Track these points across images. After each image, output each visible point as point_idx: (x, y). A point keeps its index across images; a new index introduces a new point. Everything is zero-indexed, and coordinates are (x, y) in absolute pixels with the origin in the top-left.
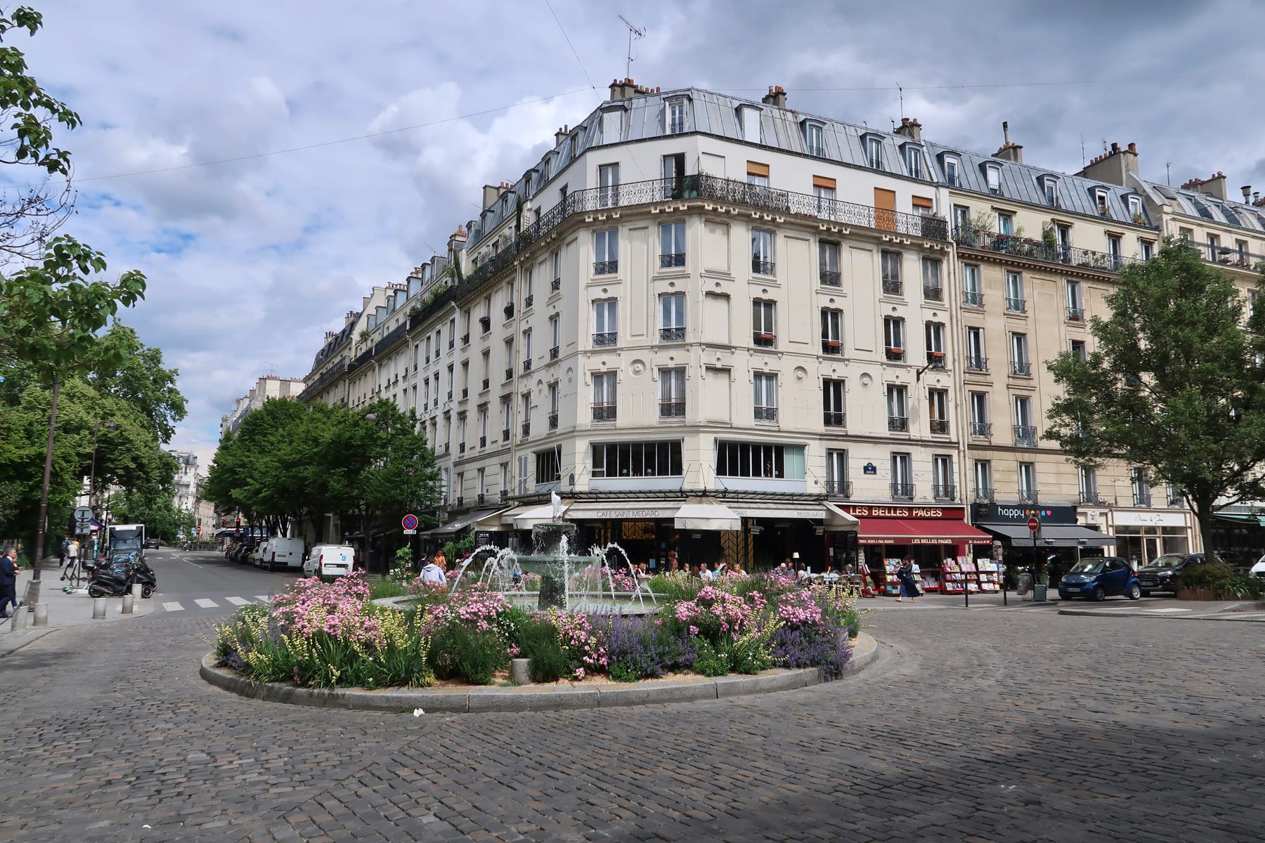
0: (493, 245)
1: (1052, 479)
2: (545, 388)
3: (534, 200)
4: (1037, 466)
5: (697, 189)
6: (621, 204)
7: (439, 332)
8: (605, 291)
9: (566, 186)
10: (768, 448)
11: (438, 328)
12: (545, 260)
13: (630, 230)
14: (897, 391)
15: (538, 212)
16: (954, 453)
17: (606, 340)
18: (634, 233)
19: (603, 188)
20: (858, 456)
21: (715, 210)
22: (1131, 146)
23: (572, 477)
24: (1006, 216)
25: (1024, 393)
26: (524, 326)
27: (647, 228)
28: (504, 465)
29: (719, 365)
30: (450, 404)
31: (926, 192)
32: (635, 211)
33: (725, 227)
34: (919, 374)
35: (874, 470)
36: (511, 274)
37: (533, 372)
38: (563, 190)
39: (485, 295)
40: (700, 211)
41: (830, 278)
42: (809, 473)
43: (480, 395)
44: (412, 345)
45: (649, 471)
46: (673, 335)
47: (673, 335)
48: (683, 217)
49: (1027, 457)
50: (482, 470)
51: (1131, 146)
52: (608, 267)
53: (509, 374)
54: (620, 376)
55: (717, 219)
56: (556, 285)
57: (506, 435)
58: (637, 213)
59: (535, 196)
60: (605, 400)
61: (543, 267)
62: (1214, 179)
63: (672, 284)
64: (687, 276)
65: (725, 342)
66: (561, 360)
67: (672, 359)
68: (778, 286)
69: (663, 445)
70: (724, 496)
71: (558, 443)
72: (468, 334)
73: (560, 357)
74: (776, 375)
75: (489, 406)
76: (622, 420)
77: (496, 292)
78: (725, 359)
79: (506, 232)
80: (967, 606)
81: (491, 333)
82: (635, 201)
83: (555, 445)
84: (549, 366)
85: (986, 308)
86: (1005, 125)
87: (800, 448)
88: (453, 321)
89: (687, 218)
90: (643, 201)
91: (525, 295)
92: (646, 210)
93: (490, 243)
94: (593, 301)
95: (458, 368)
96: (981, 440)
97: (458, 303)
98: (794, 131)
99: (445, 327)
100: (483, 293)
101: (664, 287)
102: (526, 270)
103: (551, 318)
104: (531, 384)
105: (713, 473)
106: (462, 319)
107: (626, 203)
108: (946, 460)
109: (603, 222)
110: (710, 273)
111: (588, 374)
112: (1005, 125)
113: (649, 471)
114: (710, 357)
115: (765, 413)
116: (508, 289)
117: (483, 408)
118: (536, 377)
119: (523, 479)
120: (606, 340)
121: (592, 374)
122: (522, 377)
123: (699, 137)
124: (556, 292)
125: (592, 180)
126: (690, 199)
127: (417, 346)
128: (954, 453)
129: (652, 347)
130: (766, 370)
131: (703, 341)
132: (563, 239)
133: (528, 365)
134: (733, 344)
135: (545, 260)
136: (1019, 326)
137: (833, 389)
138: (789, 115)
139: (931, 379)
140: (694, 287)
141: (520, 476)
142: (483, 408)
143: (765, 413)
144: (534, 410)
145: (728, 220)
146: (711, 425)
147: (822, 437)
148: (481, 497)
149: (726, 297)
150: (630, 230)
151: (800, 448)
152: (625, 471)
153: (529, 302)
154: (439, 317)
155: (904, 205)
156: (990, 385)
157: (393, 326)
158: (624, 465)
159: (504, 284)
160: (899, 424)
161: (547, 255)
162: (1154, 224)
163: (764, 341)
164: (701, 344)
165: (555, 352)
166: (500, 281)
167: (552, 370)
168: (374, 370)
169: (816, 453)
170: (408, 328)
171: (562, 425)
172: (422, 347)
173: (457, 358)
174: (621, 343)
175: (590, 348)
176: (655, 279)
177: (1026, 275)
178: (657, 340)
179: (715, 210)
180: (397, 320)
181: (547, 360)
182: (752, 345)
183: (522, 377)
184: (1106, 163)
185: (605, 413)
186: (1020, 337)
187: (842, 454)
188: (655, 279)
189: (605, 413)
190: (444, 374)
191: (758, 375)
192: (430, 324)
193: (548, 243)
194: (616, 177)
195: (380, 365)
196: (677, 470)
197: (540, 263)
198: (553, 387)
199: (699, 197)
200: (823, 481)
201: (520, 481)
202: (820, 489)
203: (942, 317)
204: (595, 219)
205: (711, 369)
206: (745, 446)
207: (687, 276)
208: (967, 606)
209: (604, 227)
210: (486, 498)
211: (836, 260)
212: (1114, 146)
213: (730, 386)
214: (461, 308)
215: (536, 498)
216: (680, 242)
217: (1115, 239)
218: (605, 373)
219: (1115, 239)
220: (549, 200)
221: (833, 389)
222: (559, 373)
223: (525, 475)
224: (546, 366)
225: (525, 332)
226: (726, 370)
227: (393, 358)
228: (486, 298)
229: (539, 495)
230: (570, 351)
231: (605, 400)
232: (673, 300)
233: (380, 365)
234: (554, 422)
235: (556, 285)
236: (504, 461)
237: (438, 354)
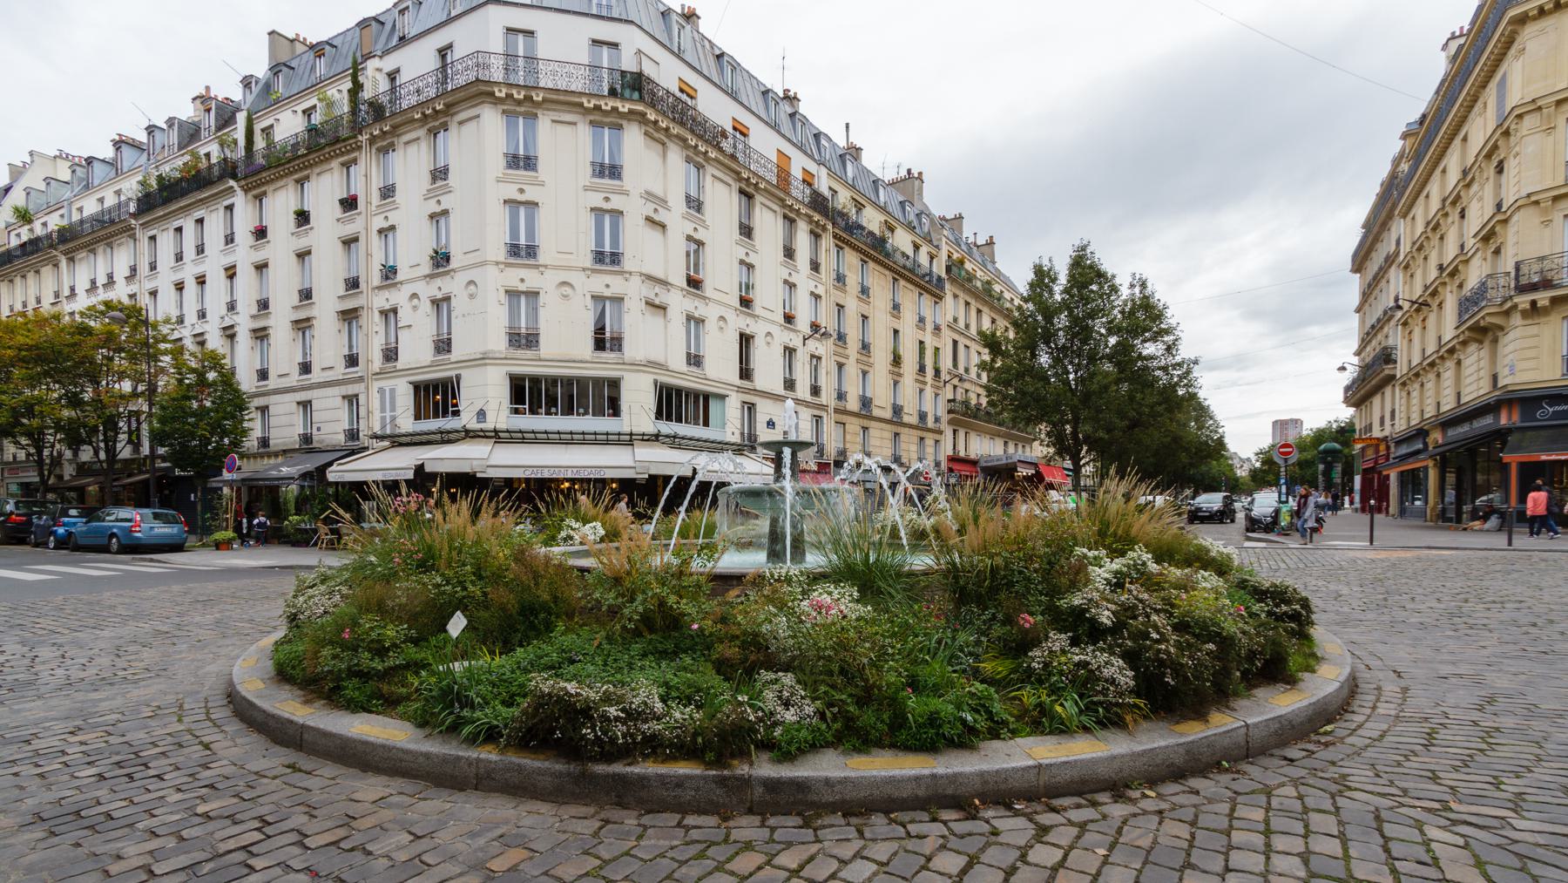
0: (304, 112)
1: (878, 443)
2: (426, 306)
3: (385, 58)
4: (871, 430)
5: (640, 90)
6: (541, 85)
7: (200, 221)
8: (521, 191)
9: (450, 46)
10: (697, 395)
11: (198, 214)
12: (418, 139)
13: (553, 121)
14: (790, 352)
15: (392, 76)
16: (824, 414)
17: (522, 252)
18: (560, 127)
19: (510, 56)
20: (765, 410)
21: (656, 122)
22: (920, 174)
23: (481, 415)
24: (860, 207)
25: (866, 368)
26: (379, 222)
27: (575, 124)
28: (352, 400)
29: (657, 302)
30: (235, 317)
31: (812, 167)
32: (562, 98)
33: (660, 146)
34: (805, 339)
35: (768, 423)
36: (353, 150)
37: (401, 283)
38: (443, 52)
39: (296, 176)
40: (641, 118)
41: (747, 231)
42: (729, 424)
43: (295, 308)
44: (143, 237)
45: (581, 411)
46: (608, 258)
47: (608, 258)
48: (620, 121)
49: (866, 423)
50: (306, 405)
51: (920, 174)
52: (522, 161)
53: (353, 284)
54: (542, 299)
55: (656, 135)
56: (440, 174)
57: (352, 361)
58: (563, 102)
59: (386, 52)
60: (523, 325)
61: (413, 149)
62: (955, 218)
63: (607, 199)
64: (626, 193)
65: (661, 275)
66: (453, 270)
67: (608, 286)
68: (707, 228)
69: (598, 382)
70: (675, 442)
71: (457, 372)
72: (233, 233)
73: (451, 267)
74: (703, 321)
75: (314, 322)
76: (547, 348)
77: (318, 174)
78: (663, 297)
79: (332, 92)
80: (1371, 543)
81: (311, 229)
82: (562, 85)
83: (453, 373)
84: (431, 276)
85: (848, 288)
86: (847, 126)
87: (723, 397)
88: (230, 208)
89: (624, 123)
90: (573, 88)
91: (377, 183)
92: (577, 100)
93: (300, 108)
94: (505, 201)
95: (191, 287)
96: (841, 405)
97: (243, 183)
98: (711, 60)
99: (214, 215)
100: (291, 173)
101: (597, 200)
102: (379, 150)
103: (432, 216)
104: (399, 297)
105: (653, 417)
106: (250, 207)
107: (550, 85)
108: (818, 419)
109: (519, 103)
110: (649, 196)
111: (502, 291)
112: (847, 126)
113: (581, 411)
114: (650, 291)
115: (695, 360)
116: (296, 190)
117: (302, 326)
118: (407, 290)
119: (388, 414)
120: (522, 252)
121: (506, 291)
122: (379, 288)
123: (634, 28)
124: (440, 183)
125: (496, 43)
126: (631, 100)
127: (153, 238)
128: (824, 414)
129: (584, 269)
130: (696, 315)
131: (644, 271)
132: (452, 115)
133: (389, 272)
134: (670, 280)
135: (418, 139)
136: (866, 310)
137: (745, 340)
138: (706, 43)
139: (815, 346)
140: (635, 210)
141: (383, 410)
142: (302, 326)
143: (695, 360)
144: (406, 330)
145: (666, 140)
146: (652, 364)
147: (740, 389)
148: (307, 439)
149: (663, 226)
150: (553, 121)
151: (723, 397)
152: (553, 410)
153: (388, 192)
154: (201, 200)
155: (796, 172)
156: (858, 361)
157: (90, 207)
158: (552, 402)
159: (335, 164)
160: (790, 384)
161: (422, 132)
162: (935, 243)
163: (694, 283)
164: (641, 274)
165: (441, 259)
166: (327, 160)
167: (438, 282)
168: (56, 266)
169: (733, 405)
170: (132, 210)
171: (457, 353)
172: (166, 241)
173: (188, 273)
174: (543, 258)
175: (502, 259)
176: (586, 189)
177: (871, 264)
178: (588, 261)
179: (656, 122)
180: (101, 200)
181: (426, 268)
182: (684, 284)
183: (379, 288)
184: (901, 184)
185: (524, 340)
186: (865, 317)
187: (751, 407)
188: (586, 189)
189: (524, 340)
190: (216, 280)
191: (689, 318)
192: (181, 208)
193: (385, 133)
194: (530, 47)
195: (71, 260)
196: (615, 410)
197: (407, 143)
198: (438, 303)
199: (641, 99)
200: (737, 433)
201: (383, 419)
202: (736, 439)
203: (820, 291)
204: (509, 96)
205: (650, 304)
206: (679, 391)
207: (626, 193)
208: (1371, 543)
209: (518, 109)
210: (315, 438)
211: (749, 213)
212: (909, 171)
213: (666, 327)
214: (246, 190)
215: (438, 437)
216: (616, 147)
217: (917, 247)
218: (523, 292)
219: (917, 247)
220: (417, 63)
221: (745, 340)
222: (451, 285)
223: (393, 409)
224: (426, 277)
225: (380, 231)
226: (662, 308)
227: (100, 250)
228: (297, 181)
229: (442, 433)
230: (472, 259)
231: (523, 325)
232: (607, 219)
233: (71, 260)
234: (443, 345)
235: (440, 174)
236: (350, 393)
237: (200, 250)
